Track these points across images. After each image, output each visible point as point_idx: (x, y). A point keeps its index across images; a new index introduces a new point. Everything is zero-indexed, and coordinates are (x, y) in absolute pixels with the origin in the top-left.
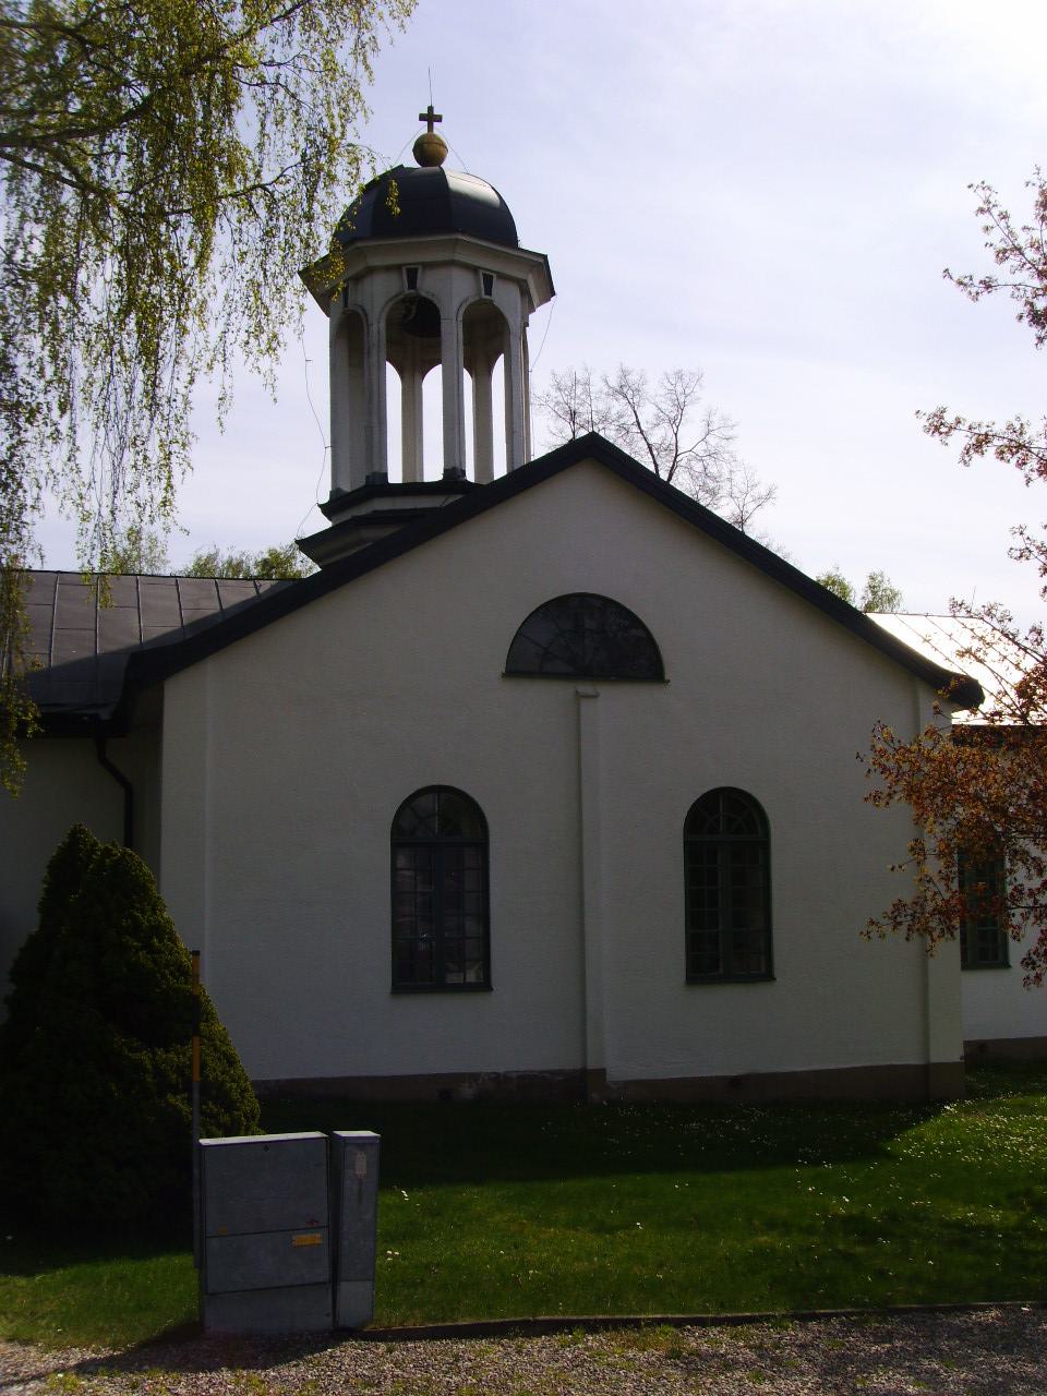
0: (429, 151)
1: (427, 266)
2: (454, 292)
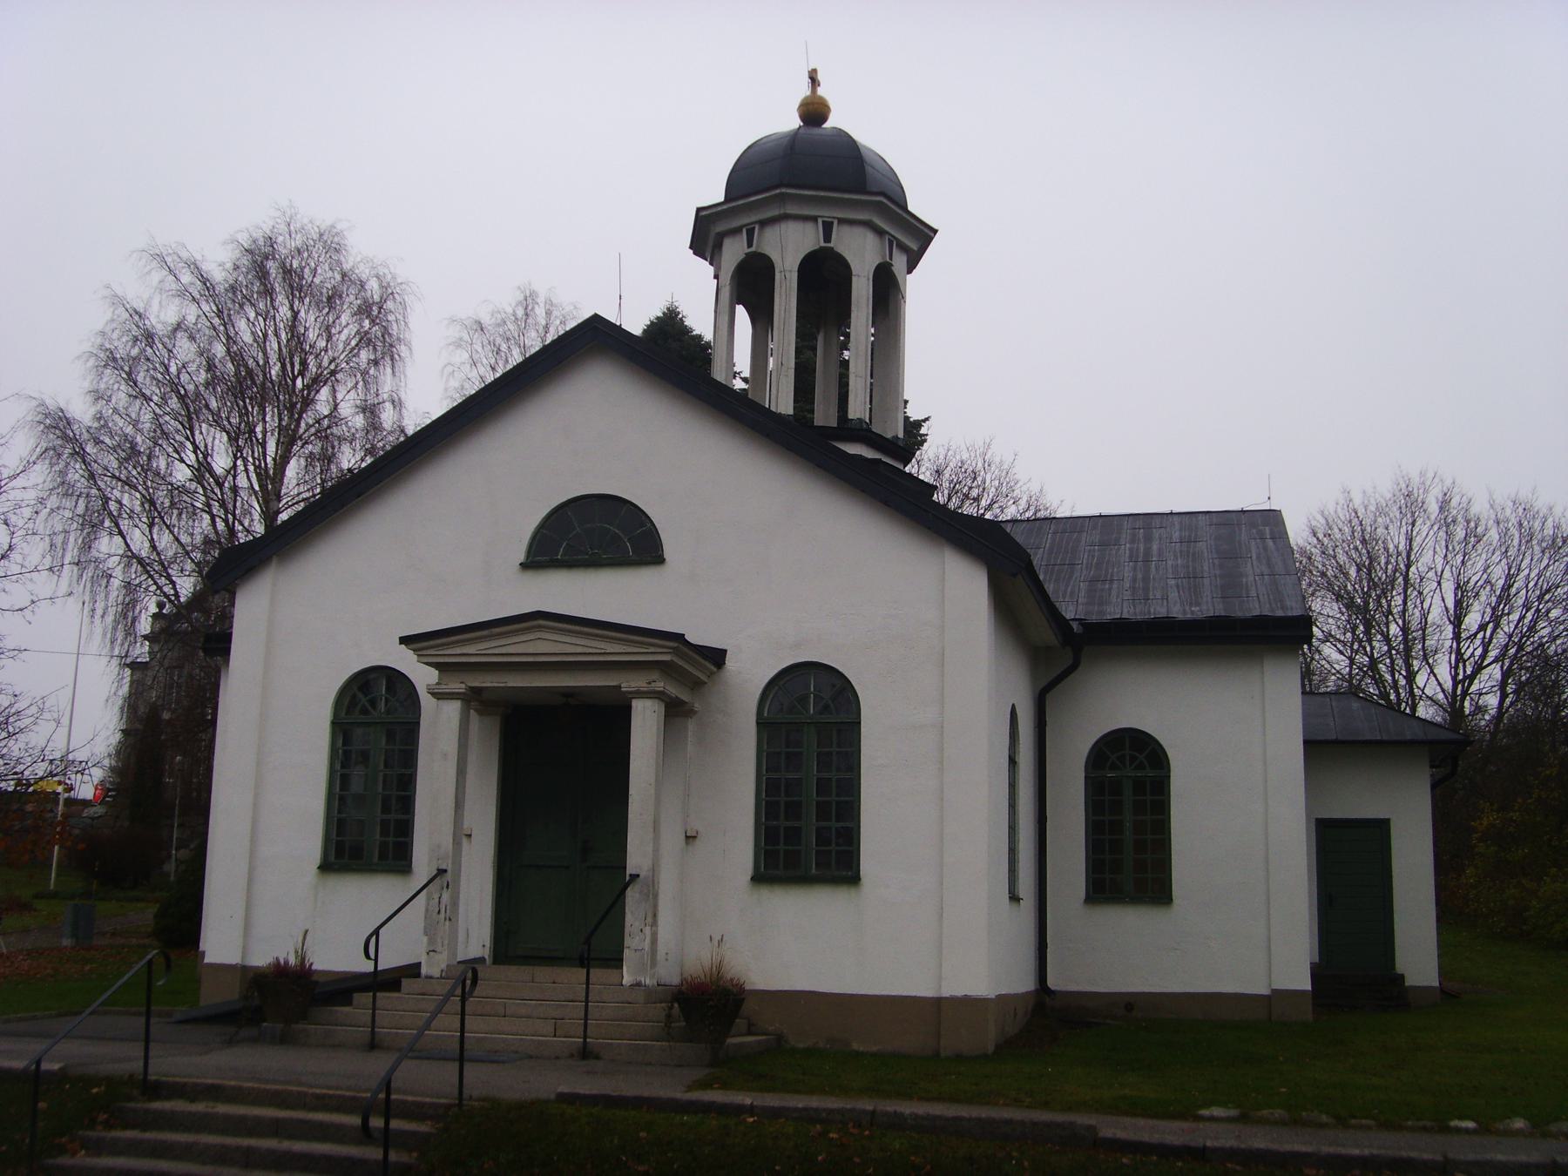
0: (814, 112)
1: (764, 224)
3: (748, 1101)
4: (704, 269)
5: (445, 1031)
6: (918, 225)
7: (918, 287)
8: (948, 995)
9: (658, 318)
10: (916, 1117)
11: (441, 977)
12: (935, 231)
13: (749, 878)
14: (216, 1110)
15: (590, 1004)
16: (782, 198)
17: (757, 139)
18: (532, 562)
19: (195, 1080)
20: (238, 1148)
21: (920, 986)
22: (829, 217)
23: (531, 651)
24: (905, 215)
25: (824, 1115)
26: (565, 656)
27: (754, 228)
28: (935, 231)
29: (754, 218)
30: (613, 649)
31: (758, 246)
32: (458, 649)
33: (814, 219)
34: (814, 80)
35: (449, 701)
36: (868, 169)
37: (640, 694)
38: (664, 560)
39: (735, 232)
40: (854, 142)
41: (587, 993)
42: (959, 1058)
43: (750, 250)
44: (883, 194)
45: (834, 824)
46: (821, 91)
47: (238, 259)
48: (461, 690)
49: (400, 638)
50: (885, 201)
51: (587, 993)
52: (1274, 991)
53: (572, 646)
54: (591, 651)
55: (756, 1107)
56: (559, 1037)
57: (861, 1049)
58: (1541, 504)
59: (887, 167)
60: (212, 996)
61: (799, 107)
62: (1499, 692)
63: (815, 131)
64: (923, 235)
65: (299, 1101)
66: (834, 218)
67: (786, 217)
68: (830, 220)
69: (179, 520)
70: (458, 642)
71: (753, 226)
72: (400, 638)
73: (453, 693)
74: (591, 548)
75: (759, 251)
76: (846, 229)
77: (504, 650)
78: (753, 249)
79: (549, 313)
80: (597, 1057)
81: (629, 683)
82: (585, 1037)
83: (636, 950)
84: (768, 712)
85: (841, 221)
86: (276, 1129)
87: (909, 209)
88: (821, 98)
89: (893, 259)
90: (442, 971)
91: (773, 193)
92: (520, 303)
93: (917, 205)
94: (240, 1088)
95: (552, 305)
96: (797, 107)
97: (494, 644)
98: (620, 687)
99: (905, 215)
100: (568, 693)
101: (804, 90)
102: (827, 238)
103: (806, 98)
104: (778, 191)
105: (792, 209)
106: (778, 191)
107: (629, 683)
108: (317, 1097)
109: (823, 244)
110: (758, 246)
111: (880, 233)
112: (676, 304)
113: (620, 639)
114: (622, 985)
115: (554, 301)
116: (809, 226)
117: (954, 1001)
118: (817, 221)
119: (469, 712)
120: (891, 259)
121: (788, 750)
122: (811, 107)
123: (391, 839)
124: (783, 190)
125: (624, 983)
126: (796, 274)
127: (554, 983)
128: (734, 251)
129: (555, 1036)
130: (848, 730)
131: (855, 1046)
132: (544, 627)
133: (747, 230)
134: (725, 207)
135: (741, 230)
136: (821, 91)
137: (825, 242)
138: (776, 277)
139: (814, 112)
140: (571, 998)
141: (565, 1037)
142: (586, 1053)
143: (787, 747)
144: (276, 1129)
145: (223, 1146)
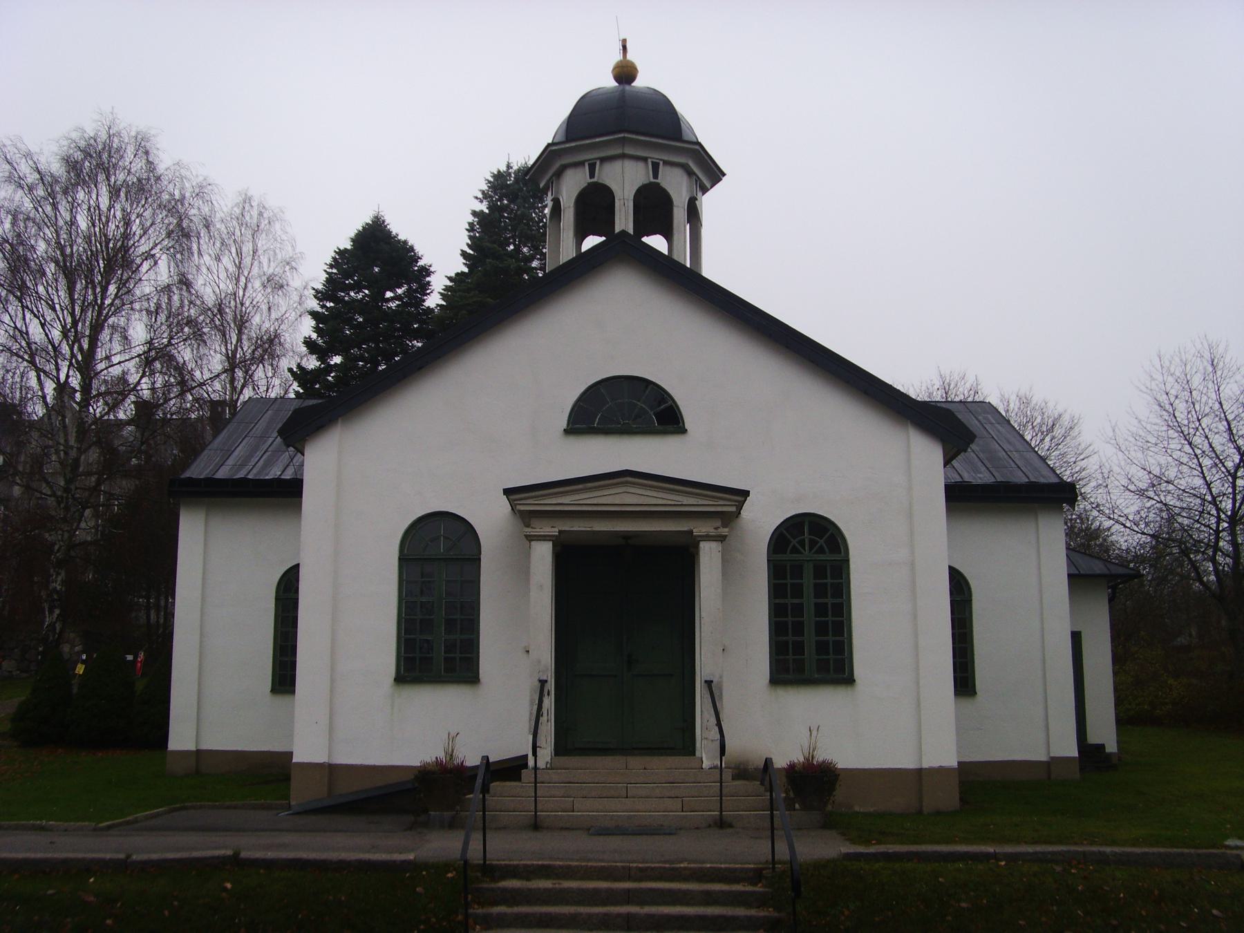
0: (625, 73)
1: (603, 160)
2: (676, 185)
3: (991, 850)
5: (593, 812)
7: (709, 203)
8: (927, 767)
10: (1115, 854)
11: (547, 768)
12: (724, 175)
13: (768, 681)
14: (562, 886)
15: (538, 785)
16: (623, 142)
17: (589, 90)
18: (571, 429)
19: (507, 862)
20: (619, 915)
21: (904, 760)
22: (657, 159)
25: (1049, 856)
26: (593, 506)
27: (596, 163)
28: (724, 175)
30: (689, 502)
32: (549, 500)
33: (645, 159)
35: (542, 542)
37: (708, 538)
38: (686, 430)
42: (938, 813)
45: (791, 638)
47: (36, 153)
48: (554, 533)
50: (700, 150)
52: (1052, 758)
53: (655, 499)
54: (670, 502)
55: (999, 853)
56: (686, 812)
57: (861, 810)
58: (1037, 399)
60: (300, 794)
61: (613, 70)
63: (627, 87)
65: (627, 875)
66: (661, 160)
67: (623, 156)
68: (657, 161)
71: (595, 161)
73: (540, 536)
74: (622, 419)
75: (600, 181)
76: (668, 168)
78: (595, 180)
79: (261, 214)
80: (731, 826)
81: (700, 528)
82: (721, 811)
83: (712, 741)
84: (407, 550)
85: (666, 163)
86: (628, 897)
90: (547, 763)
91: (616, 136)
92: (237, 205)
94: (569, 867)
95: (264, 207)
96: (611, 69)
97: (577, 497)
98: (691, 532)
100: (627, 536)
101: (618, 57)
102: (656, 175)
104: (622, 135)
106: (622, 135)
107: (700, 528)
108: (641, 869)
109: (652, 180)
110: (599, 177)
111: (690, 173)
112: (383, 214)
113: (697, 494)
114: (702, 768)
115: (267, 206)
116: (641, 165)
117: (932, 771)
119: (528, 555)
121: (423, 580)
122: (625, 69)
124: (626, 135)
125: (704, 767)
127: (645, 769)
129: (682, 811)
130: (840, 568)
131: (857, 809)
132: (630, 483)
133: (589, 164)
134: (563, 146)
135: (584, 165)
136: (630, 57)
137: (654, 178)
138: (616, 205)
139: (625, 73)
140: (671, 780)
141: (691, 812)
142: (722, 824)
143: (422, 578)
144: (628, 897)
145: (605, 914)
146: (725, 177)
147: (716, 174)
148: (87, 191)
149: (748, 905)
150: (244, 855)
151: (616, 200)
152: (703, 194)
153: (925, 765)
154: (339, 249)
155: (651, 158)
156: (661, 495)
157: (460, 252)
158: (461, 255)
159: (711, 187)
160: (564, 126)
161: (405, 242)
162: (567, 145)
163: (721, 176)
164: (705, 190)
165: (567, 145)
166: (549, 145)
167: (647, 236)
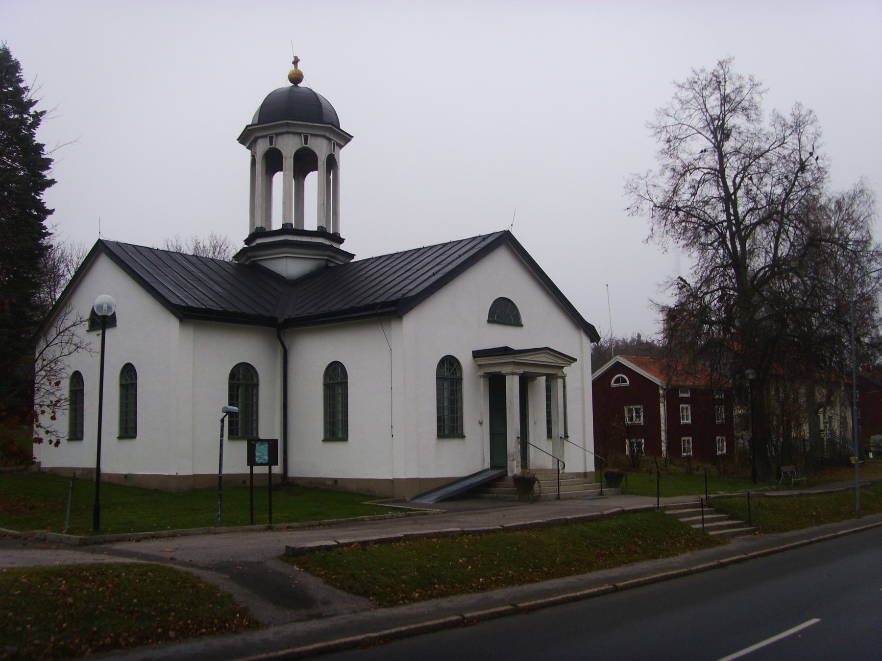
0: (296, 78)
1: (278, 135)
2: (320, 148)
4: (245, 154)
6: (346, 136)
7: (344, 155)
9: (40, 147)
12: (352, 137)
16: (288, 125)
23: (542, 360)
24: (339, 131)
27: (273, 136)
29: (273, 132)
31: (275, 145)
33: (300, 134)
34: (296, 62)
36: (324, 110)
37: (513, 374)
39: (265, 137)
40: (315, 94)
41: (558, 477)
43: (271, 146)
44: (332, 124)
46: (299, 68)
49: (474, 352)
51: (558, 477)
59: (331, 107)
62: (37, 370)
64: (347, 138)
67: (288, 133)
69: (857, 349)
70: (525, 356)
72: (474, 352)
77: (534, 359)
78: (273, 146)
82: (559, 492)
85: (312, 135)
87: (341, 128)
88: (299, 71)
89: (335, 151)
93: (345, 126)
97: (535, 356)
99: (339, 131)
102: (306, 143)
103: (292, 71)
104: (285, 121)
105: (292, 130)
106: (285, 121)
111: (329, 140)
118: (301, 136)
120: (334, 152)
123: (455, 424)
126: (293, 159)
128: (263, 146)
133: (269, 137)
139: (296, 78)
146: (353, 138)
147: (347, 138)
148: (700, 264)
149: (713, 514)
150: (341, 541)
151: (319, 161)
152: (340, 149)
153: (587, 471)
154: (36, 123)
155: (304, 133)
156: (555, 359)
157: (56, 180)
158: (54, 179)
159: (345, 145)
160: (257, 116)
161: (51, 186)
162: (259, 126)
163: (350, 138)
164: (341, 147)
165: (259, 126)
166: (248, 126)
167: (312, 171)
